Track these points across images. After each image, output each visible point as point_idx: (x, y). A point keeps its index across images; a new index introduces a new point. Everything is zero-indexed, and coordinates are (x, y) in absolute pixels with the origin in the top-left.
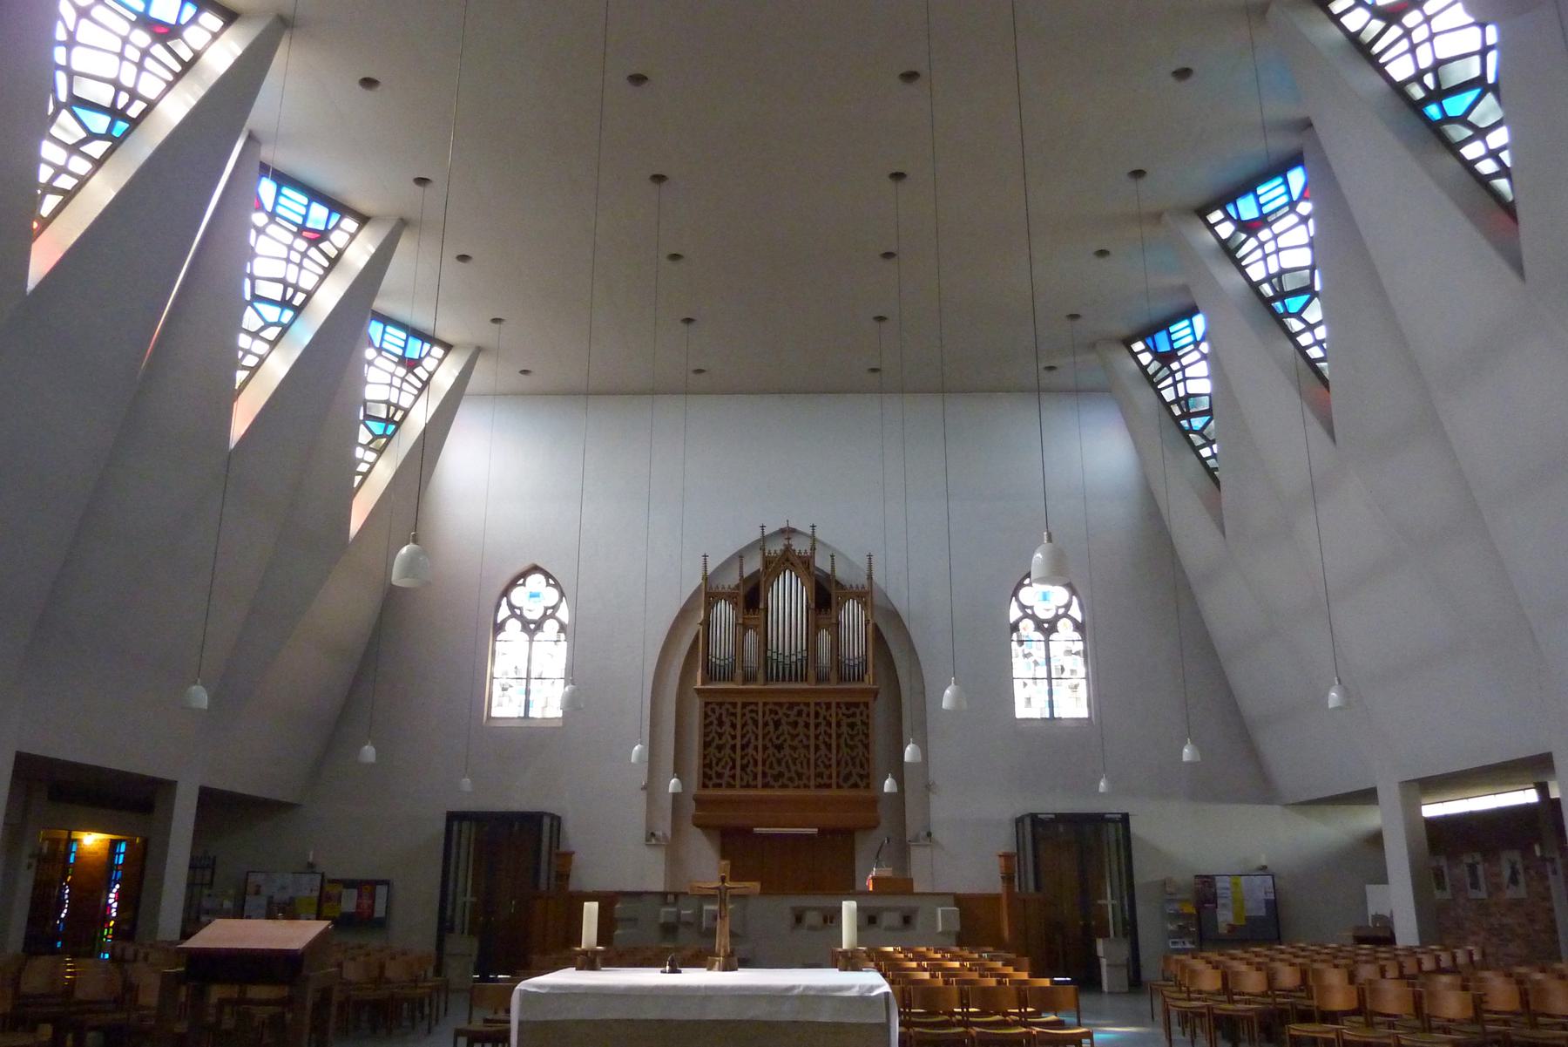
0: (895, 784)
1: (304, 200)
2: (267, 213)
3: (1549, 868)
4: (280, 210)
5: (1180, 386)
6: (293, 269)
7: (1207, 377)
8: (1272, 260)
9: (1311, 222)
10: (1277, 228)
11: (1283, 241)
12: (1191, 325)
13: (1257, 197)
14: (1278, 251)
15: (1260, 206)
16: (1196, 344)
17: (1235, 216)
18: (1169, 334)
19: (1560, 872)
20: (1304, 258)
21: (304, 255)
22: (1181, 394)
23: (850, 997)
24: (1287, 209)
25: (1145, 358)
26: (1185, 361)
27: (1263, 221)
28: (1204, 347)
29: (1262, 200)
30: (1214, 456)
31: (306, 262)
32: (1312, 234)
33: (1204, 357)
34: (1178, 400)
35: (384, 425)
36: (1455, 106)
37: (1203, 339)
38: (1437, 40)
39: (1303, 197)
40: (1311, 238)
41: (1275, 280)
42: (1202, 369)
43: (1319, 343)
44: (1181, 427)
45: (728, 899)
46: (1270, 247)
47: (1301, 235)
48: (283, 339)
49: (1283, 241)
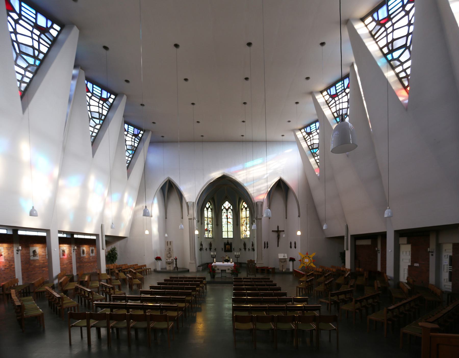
0: (302, 164)
1: (133, 128)
2: (127, 132)
3: (378, 252)
4: (94, 92)
5: (312, 141)
6: (101, 109)
7: (318, 139)
8: (338, 106)
9: (349, 95)
10: (340, 97)
11: (314, 138)
12: (316, 125)
13: (336, 87)
14: (313, 139)
15: (336, 90)
16: (316, 130)
17: (330, 94)
18: (310, 128)
19: (380, 253)
20: (345, 105)
21: (103, 105)
22: (312, 143)
23: (233, 214)
24: (401, 9)
25: (304, 134)
26: (313, 135)
27: (336, 95)
28: (318, 131)
29: (337, 89)
30: (318, 159)
31: (104, 107)
32: (349, 98)
33: (318, 134)
34: (311, 145)
35: (131, 151)
36: (396, 54)
37: (318, 129)
38: (314, 140)
39: (348, 87)
40: (348, 100)
41: (390, 45)
42: (317, 137)
43: (318, 159)
44: (311, 151)
45: (75, 312)
46: (337, 102)
47: (345, 99)
48: (101, 128)
49: (314, 138)
